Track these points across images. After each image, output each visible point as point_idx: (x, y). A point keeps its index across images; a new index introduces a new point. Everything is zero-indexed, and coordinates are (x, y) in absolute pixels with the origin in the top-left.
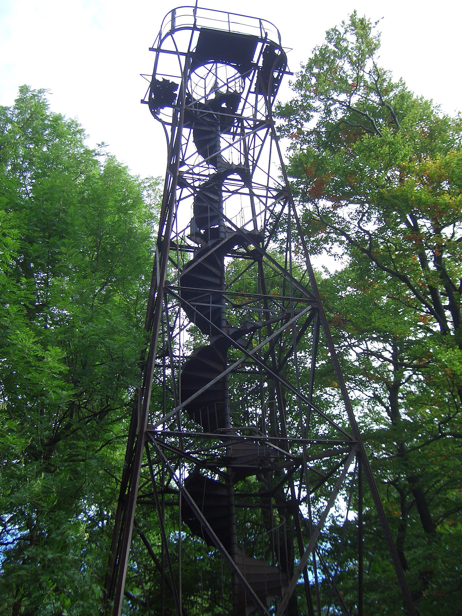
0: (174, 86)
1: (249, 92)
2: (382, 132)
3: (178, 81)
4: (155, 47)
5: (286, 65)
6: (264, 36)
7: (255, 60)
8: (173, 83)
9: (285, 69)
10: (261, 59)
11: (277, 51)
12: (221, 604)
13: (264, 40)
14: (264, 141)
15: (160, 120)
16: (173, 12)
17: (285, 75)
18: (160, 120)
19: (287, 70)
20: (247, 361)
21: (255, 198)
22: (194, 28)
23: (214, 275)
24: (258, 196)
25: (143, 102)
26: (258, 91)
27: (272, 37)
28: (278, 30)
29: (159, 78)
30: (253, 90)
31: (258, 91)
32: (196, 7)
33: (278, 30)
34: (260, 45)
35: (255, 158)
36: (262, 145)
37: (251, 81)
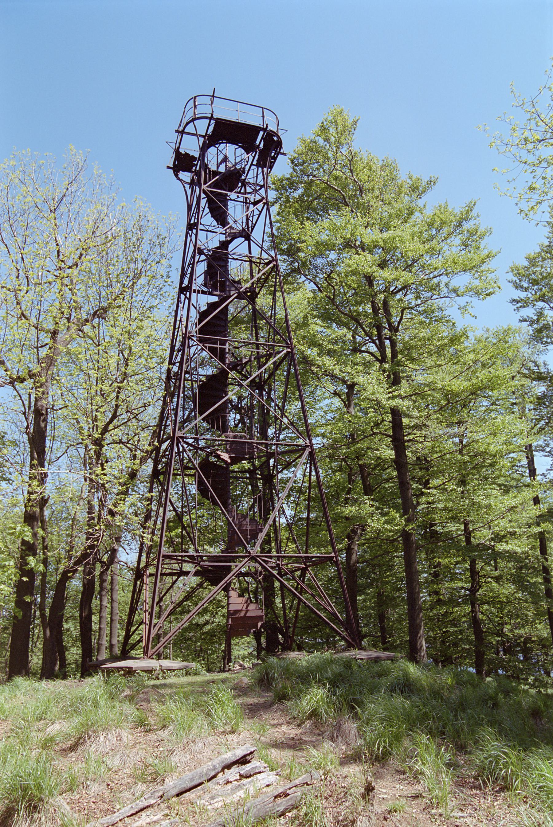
0: (194, 158)
1: (252, 164)
2: (270, 564)
3: (197, 155)
4: (180, 129)
5: (281, 147)
6: (265, 126)
7: (257, 142)
8: (193, 156)
9: (280, 150)
10: (262, 143)
11: (275, 139)
12: (286, 602)
13: (265, 130)
14: (261, 212)
15: (181, 180)
16: (195, 97)
17: (280, 156)
18: (181, 180)
19: (282, 151)
20: (295, 811)
21: (253, 264)
22: (211, 118)
23: (223, 320)
24: (254, 262)
25: (168, 167)
26: (258, 165)
27: (272, 127)
28: (277, 120)
29: (182, 151)
30: (255, 163)
31: (258, 165)
32: (213, 96)
33: (277, 120)
34: (261, 133)
35: (254, 222)
36: (260, 215)
37: (254, 157)
